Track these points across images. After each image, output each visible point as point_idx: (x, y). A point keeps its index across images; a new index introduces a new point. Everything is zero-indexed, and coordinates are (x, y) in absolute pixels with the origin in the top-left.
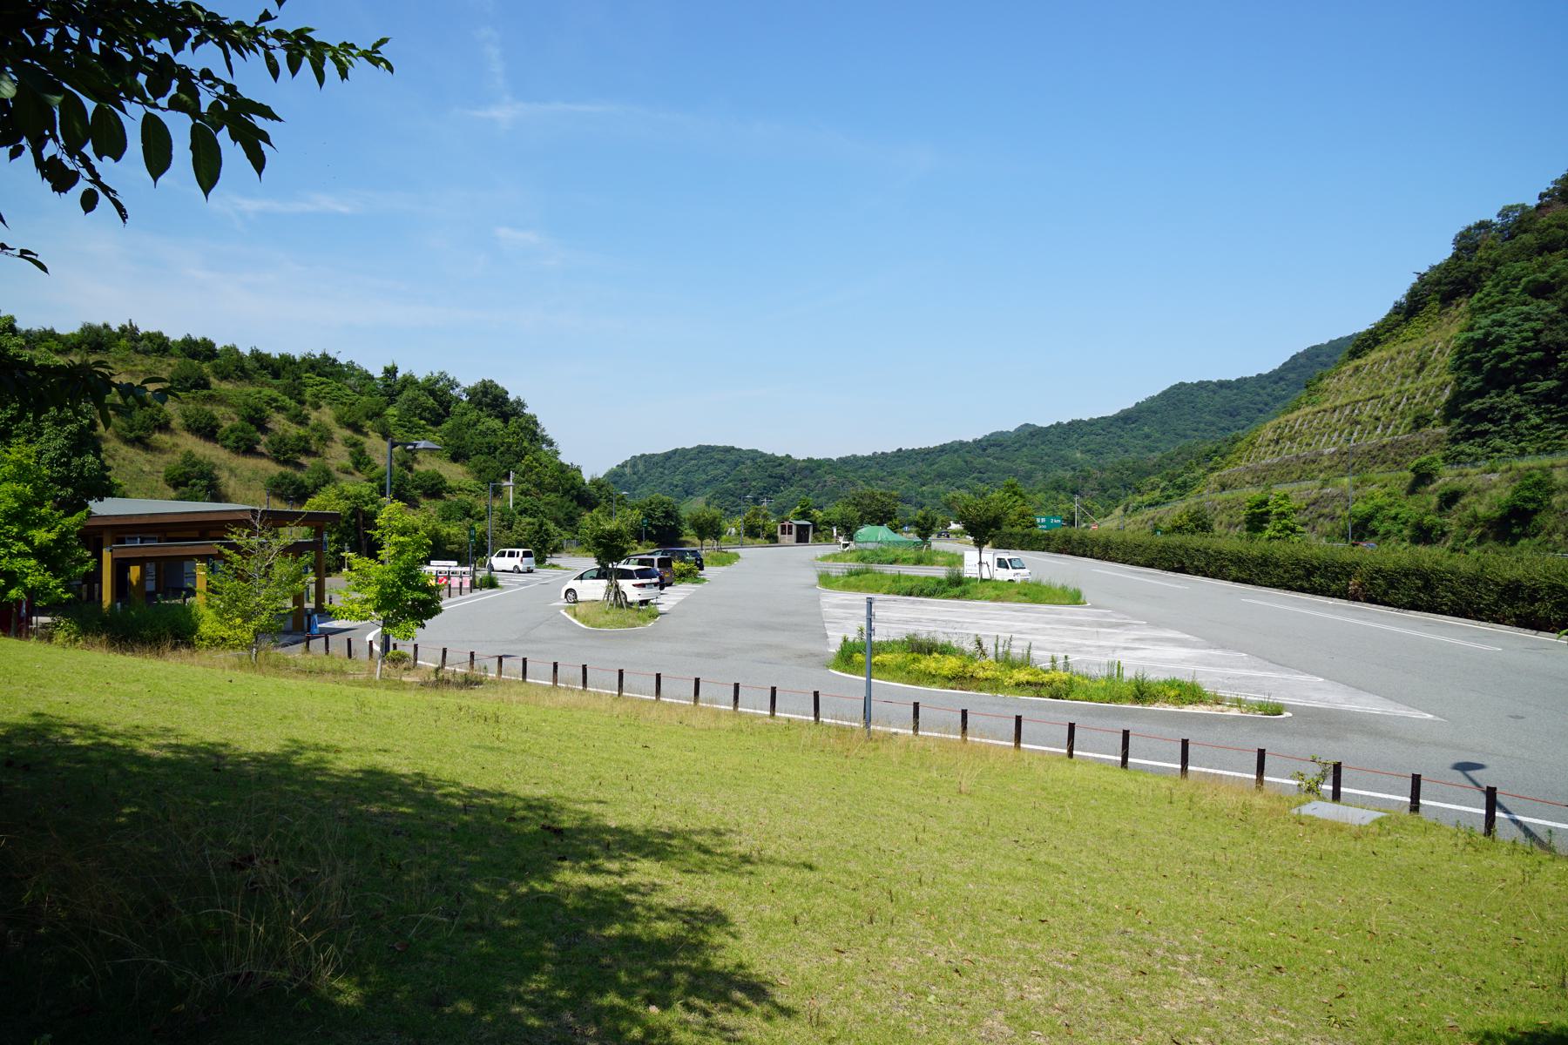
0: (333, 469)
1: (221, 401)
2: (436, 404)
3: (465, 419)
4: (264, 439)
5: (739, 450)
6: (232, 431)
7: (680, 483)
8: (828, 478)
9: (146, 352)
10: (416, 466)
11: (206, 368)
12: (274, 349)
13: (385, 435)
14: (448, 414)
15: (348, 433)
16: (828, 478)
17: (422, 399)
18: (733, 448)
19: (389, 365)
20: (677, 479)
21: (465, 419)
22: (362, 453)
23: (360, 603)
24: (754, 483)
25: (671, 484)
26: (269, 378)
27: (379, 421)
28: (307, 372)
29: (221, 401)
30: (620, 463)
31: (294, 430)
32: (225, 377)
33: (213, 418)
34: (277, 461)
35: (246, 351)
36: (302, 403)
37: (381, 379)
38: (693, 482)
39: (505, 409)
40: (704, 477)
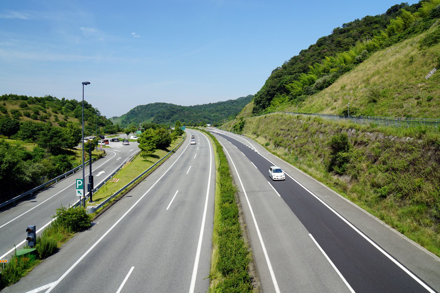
0: (51, 122)
1: (30, 109)
2: (73, 106)
3: (79, 109)
4: (39, 116)
5: (167, 104)
6: (33, 116)
7: (150, 113)
8: (186, 112)
9: (14, 100)
10: (68, 120)
11: (26, 102)
12: (39, 96)
13: (62, 114)
14: (75, 108)
15: (54, 114)
16: (186, 112)
17: (70, 105)
18: (165, 103)
19: (63, 98)
20: (149, 112)
21: (79, 109)
22: (57, 118)
23: (222, 186)
24: (166, 114)
25: (147, 113)
26: (38, 103)
27: (61, 111)
28: (46, 100)
29: (30, 109)
30: (134, 108)
31: (44, 114)
32: (30, 104)
33: (29, 113)
34: (41, 120)
35: (33, 97)
36: (45, 108)
37: (61, 100)
38: (153, 113)
39: (87, 106)
40: (157, 111)
